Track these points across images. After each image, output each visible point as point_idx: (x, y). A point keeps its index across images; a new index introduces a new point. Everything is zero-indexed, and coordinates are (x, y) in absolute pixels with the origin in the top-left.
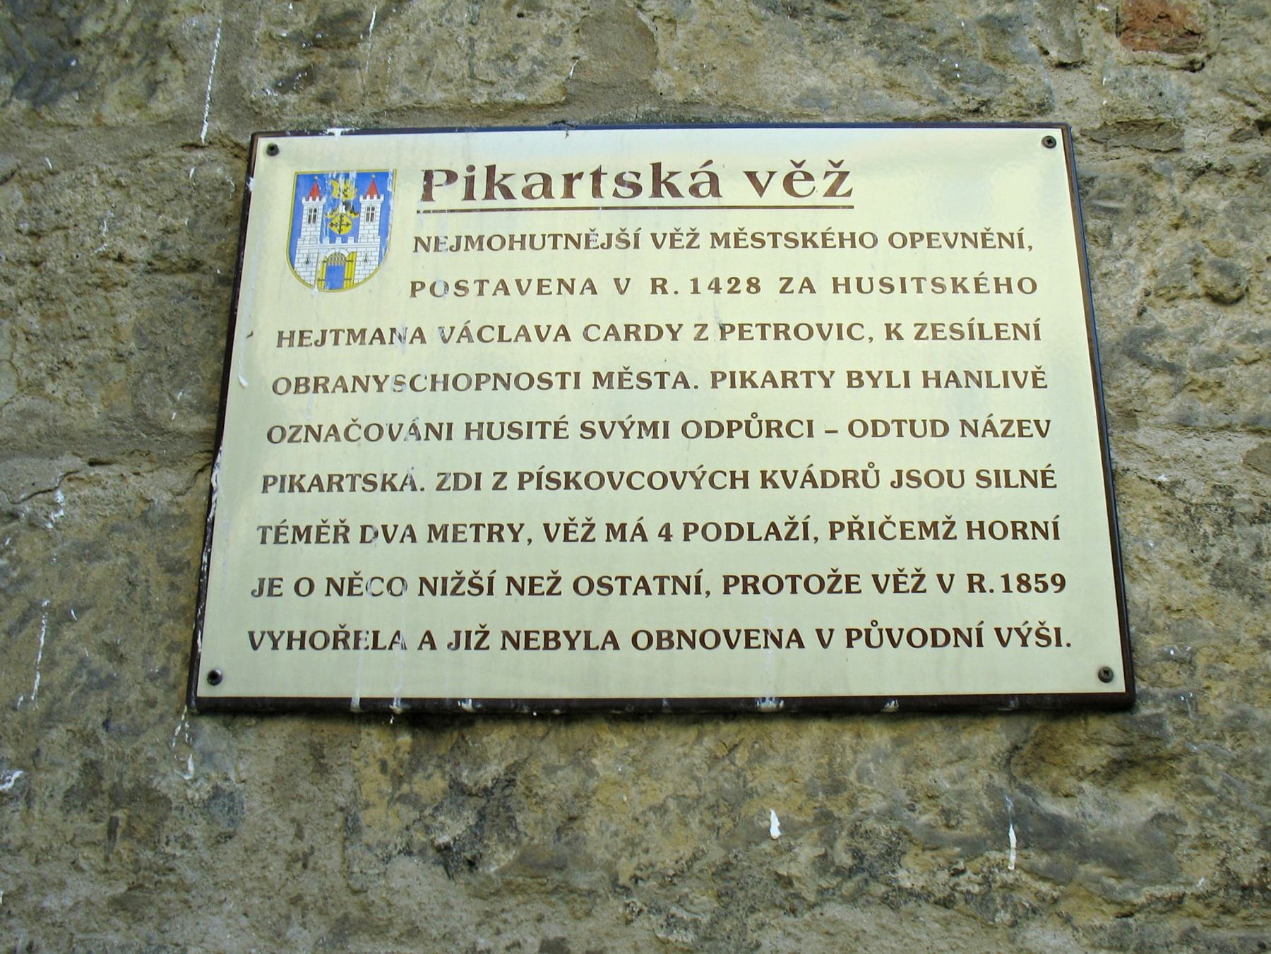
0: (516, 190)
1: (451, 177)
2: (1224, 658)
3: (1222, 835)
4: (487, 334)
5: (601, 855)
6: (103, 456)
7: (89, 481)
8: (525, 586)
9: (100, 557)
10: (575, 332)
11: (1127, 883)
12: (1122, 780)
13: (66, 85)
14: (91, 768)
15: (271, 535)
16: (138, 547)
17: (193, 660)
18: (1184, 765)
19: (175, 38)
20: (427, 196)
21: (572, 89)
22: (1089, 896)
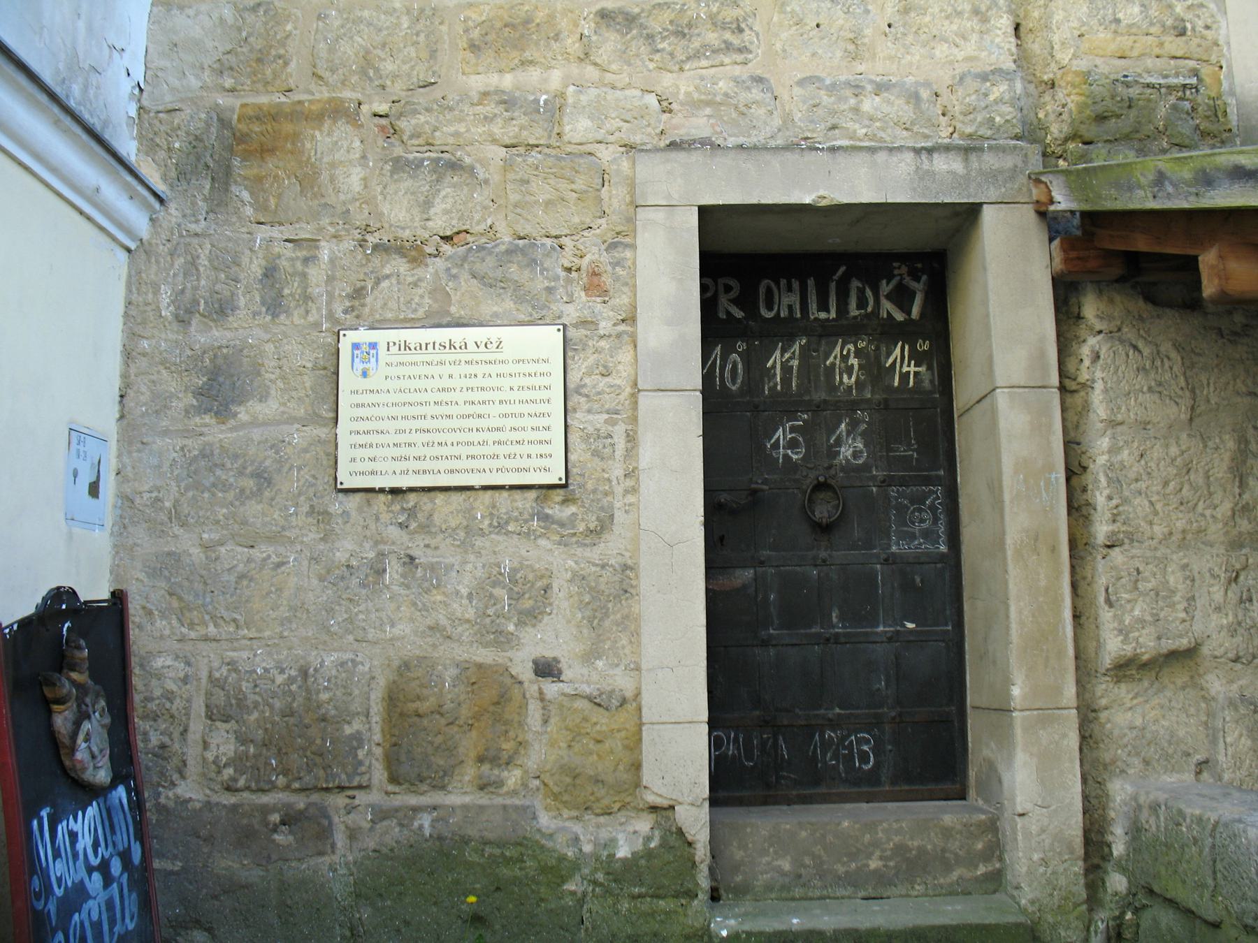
0: (412, 348)
8: (417, 458)
14: (312, 506)
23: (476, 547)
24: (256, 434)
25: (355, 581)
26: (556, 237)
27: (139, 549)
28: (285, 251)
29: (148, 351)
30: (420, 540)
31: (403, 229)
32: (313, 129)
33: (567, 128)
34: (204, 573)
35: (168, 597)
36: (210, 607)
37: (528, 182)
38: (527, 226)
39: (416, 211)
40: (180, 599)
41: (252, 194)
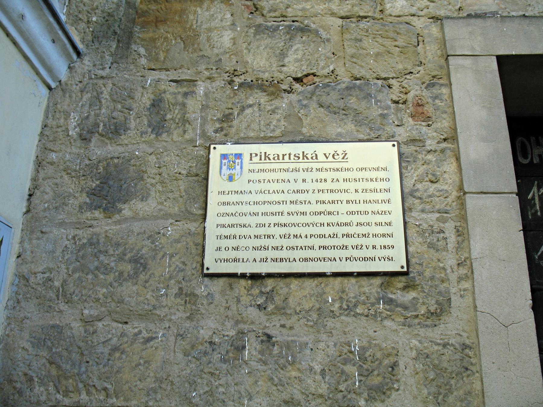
1: (256, 155)
2: (430, 264)
3: (427, 302)
4: (266, 192)
5: (293, 306)
6: (179, 220)
7: (176, 225)
9: (179, 242)
10: (286, 192)
11: (406, 312)
12: (406, 290)
13: (164, 131)
14: (181, 289)
15: (219, 237)
16: (188, 240)
17: (202, 265)
18: (419, 287)
19: (189, 120)
20: (251, 160)
21: (283, 133)
22: (398, 315)
23: (328, 328)
24: (136, 227)
25: (216, 357)
26: (385, 79)
27: (28, 321)
28: (169, 88)
29: (55, 160)
30: (277, 320)
31: (264, 72)
32: (196, 6)
33: (388, 6)
34: (81, 344)
35: (48, 365)
36: (84, 376)
37: (361, 40)
38: (362, 71)
39: (273, 60)
40: (59, 367)
41: (146, 50)
